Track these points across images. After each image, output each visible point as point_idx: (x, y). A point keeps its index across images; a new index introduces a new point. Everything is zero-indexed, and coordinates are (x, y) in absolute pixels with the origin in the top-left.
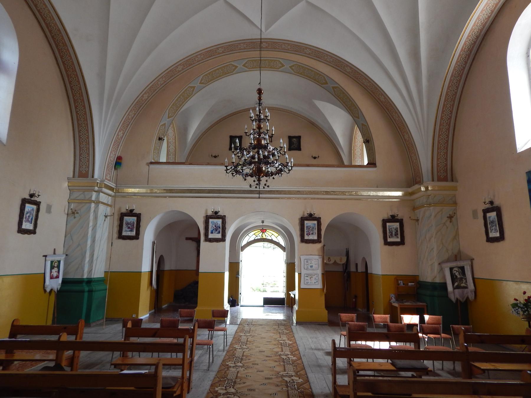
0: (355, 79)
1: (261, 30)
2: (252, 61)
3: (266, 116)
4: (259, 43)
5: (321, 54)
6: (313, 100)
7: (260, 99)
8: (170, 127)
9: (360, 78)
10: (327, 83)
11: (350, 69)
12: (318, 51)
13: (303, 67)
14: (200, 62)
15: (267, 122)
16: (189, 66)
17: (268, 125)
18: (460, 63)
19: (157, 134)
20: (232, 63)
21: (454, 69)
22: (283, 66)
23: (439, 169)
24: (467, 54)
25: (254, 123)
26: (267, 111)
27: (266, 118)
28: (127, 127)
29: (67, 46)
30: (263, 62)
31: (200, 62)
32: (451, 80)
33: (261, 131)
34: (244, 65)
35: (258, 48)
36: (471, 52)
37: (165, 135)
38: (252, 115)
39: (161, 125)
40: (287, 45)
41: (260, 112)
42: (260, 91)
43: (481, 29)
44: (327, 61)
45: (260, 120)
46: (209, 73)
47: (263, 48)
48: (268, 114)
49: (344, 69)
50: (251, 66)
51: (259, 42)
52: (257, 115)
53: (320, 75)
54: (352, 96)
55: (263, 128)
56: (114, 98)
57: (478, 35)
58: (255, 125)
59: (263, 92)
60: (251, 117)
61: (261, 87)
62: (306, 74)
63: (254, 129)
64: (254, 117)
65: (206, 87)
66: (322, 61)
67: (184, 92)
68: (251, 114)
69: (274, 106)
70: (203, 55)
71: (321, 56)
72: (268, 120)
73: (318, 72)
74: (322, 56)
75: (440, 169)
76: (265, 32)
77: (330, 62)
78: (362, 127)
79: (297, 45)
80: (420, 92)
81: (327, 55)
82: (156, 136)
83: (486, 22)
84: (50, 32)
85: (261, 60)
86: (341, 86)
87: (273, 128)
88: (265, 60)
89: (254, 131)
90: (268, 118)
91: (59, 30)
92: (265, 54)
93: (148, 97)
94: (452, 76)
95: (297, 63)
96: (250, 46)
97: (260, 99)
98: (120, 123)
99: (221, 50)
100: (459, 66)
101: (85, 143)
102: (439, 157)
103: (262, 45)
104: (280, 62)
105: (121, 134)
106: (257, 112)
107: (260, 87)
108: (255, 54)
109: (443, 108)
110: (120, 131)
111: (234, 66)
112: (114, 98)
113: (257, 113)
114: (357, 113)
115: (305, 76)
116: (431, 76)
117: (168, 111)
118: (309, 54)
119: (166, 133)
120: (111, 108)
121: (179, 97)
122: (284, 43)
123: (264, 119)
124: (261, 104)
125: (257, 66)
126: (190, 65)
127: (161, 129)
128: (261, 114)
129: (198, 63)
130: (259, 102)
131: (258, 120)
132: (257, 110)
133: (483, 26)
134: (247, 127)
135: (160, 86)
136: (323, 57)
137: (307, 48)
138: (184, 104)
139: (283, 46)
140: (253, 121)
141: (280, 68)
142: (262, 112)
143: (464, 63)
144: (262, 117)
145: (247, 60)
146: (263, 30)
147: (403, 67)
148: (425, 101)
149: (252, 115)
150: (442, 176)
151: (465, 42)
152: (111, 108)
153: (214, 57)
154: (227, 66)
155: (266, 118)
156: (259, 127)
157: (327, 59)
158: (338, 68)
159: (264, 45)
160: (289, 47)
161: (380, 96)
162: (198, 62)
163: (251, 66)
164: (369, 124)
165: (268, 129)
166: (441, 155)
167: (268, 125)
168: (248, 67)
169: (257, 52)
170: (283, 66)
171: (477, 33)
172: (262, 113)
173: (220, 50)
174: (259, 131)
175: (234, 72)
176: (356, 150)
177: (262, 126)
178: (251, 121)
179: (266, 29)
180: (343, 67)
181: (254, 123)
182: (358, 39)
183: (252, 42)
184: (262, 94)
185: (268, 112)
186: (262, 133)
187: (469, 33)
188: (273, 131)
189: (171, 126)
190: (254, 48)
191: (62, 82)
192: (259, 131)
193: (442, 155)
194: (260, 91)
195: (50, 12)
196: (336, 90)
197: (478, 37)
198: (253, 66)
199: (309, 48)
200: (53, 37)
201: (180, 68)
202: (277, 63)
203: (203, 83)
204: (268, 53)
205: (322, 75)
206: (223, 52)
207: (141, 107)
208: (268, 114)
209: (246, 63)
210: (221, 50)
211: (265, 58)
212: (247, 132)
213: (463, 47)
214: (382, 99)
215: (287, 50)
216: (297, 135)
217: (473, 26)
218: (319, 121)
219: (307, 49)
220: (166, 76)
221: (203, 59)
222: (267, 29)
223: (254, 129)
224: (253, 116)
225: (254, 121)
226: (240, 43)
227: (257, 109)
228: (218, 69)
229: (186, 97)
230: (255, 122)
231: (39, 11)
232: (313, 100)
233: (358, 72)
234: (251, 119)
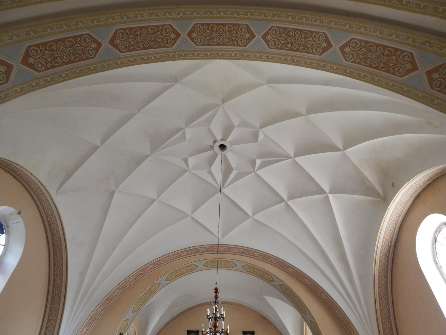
0: (298, 278)
1: (218, 238)
2: (211, 261)
3: (222, 315)
4: (216, 248)
5: (267, 257)
6: (264, 296)
7: (216, 298)
8: (133, 322)
9: (301, 278)
10: (273, 281)
11: (292, 269)
12: (264, 255)
13: (253, 267)
14: (167, 262)
15: (222, 321)
16: (159, 266)
17: (224, 324)
18: (382, 267)
19: (120, 330)
20: (194, 263)
21: (379, 272)
22: (236, 266)
23: (381, 297)
24: (386, 260)
25: (211, 322)
26: (222, 310)
27: (222, 317)
28: (93, 322)
29: (62, 251)
30: (219, 263)
31: (167, 262)
32: (379, 282)
33: (217, 329)
34: (204, 265)
35: (216, 251)
36: (388, 258)
37: (126, 330)
38: (209, 313)
39: (125, 320)
40: (239, 250)
41: (216, 311)
42: (216, 291)
43: (390, 241)
44: (272, 262)
45: (216, 318)
46: (174, 272)
47: (220, 251)
48: (223, 312)
49: (287, 269)
50: (209, 266)
51: (216, 247)
52: (214, 313)
53: (268, 274)
54: (296, 292)
55: (219, 327)
56: (88, 294)
57: (390, 245)
58: (211, 323)
59: (219, 291)
60: (208, 316)
61: (217, 287)
62: (255, 273)
63: (210, 328)
64: (210, 316)
65: (170, 283)
66: (269, 262)
67: (150, 289)
68: (208, 313)
69: (229, 301)
70: (171, 256)
71: (267, 258)
72: (223, 318)
73: (266, 271)
74: (268, 258)
75: (381, 298)
76: (222, 239)
77: (275, 264)
78: (311, 324)
79: (247, 250)
80: (355, 291)
81: (272, 258)
82: (118, 331)
83: (392, 236)
84: (53, 240)
85: (218, 247)
86: (286, 284)
87: (228, 327)
88: (222, 261)
89: (210, 330)
90: (224, 316)
91: (60, 239)
92: (221, 256)
93: (119, 293)
94: (379, 278)
95: (248, 264)
96: (209, 250)
97: (216, 298)
98: (87, 319)
99: (186, 253)
100: (382, 269)
101: (53, 315)
102: (382, 308)
103: (219, 249)
104: (234, 263)
105: (85, 330)
106: (214, 311)
107: (216, 287)
108: (213, 256)
109: (380, 307)
110: (85, 327)
111: (195, 265)
112: (88, 294)
113: (214, 312)
114: (304, 309)
115: (254, 274)
116: (361, 279)
117: (133, 306)
118: (257, 257)
119: (127, 328)
120: (83, 303)
121: (146, 293)
122: (237, 248)
123: (219, 318)
124: (217, 302)
125: (214, 266)
126: (159, 265)
127: (124, 324)
128: (217, 312)
129: (166, 263)
130: (216, 300)
131: (214, 318)
132: (214, 309)
133: (391, 239)
134: (203, 325)
135: (131, 283)
136: (269, 259)
137: (256, 252)
138: (149, 299)
139: (236, 250)
140: (209, 319)
141: (233, 267)
142: (218, 310)
143: (386, 267)
144: (218, 315)
145: (206, 261)
146: (220, 238)
147: (334, 266)
148: (364, 307)
149: (209, 313)
150: (383, 282)
151: (381, 251)
152: (83, 303)
153: (180, 258)
154: (190, 265)
155: (222, 317)
156: (215, 326)
157: (272, 261)
158: (282, 268)
159: (220, 249)
160: (241, 251)
161: (322, 294)
162: (166, 262)
163: (209, 266)
164: (316, 320)
165: (223, 328)
166: (387, 330)
167: (223, 324)
168: (207, 266)
169: (215, 254)
170: (236, 266)
171: (388, 244)
172: (218, 312)
173: (186, 253)
174: (215, 330)
175: (195, 271)
176: (308, 331)
177: (218, 325)
178: (208, 320)
179: (222, 238)
180: (286, 268)
181: (211, 322)
182: (295, 245)
183: (211, 247)
184: (218, 293)
185: (223, 311)
186: (218, 332)
187: (382, 244)
188: (228, 329)
189: (134, 320)
190: (212, 251)
191: (47, 280)
192: (215, 330)
193: (388, 330)
194: (216, 291)
195: (57, 226)
196: (282, 287)
197: (390, 247)
198: (211, 266)
199: (257, 252)
200: (53, 244)
201: (150, 267)
202: (232, 263)
203: (168, 280)
204: (224, 255)
205: (269, 274)
206: (188, 255)
207: (110, 302)
208: (223, 312)
209: (205, 263)
210: (186, 253)
211: (221, 260)
212: (203, 330)
213: (380, 255)
214: (324, 296)
215: (239, 253)
216: (250, 330)
217: (383, 239)
218: (270, 316)
219: (255, 253)
220: (137, 274)
221: (170, 260)
222: (223, 237)
223: (210, 328)
224: (209, 314)
225: (211, 320)
226: (202, 248)
227: (214, 307)
228: (182, 268)
229: (151, 293)
230: (211, 320)
231: (49, 225)
232: (264, 296)
233: (299, 272)
234: (208, 317)
